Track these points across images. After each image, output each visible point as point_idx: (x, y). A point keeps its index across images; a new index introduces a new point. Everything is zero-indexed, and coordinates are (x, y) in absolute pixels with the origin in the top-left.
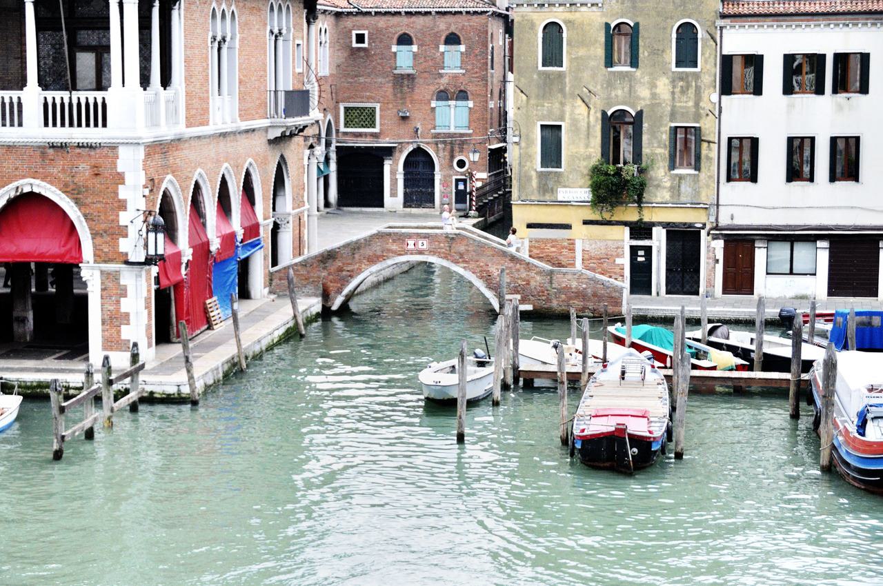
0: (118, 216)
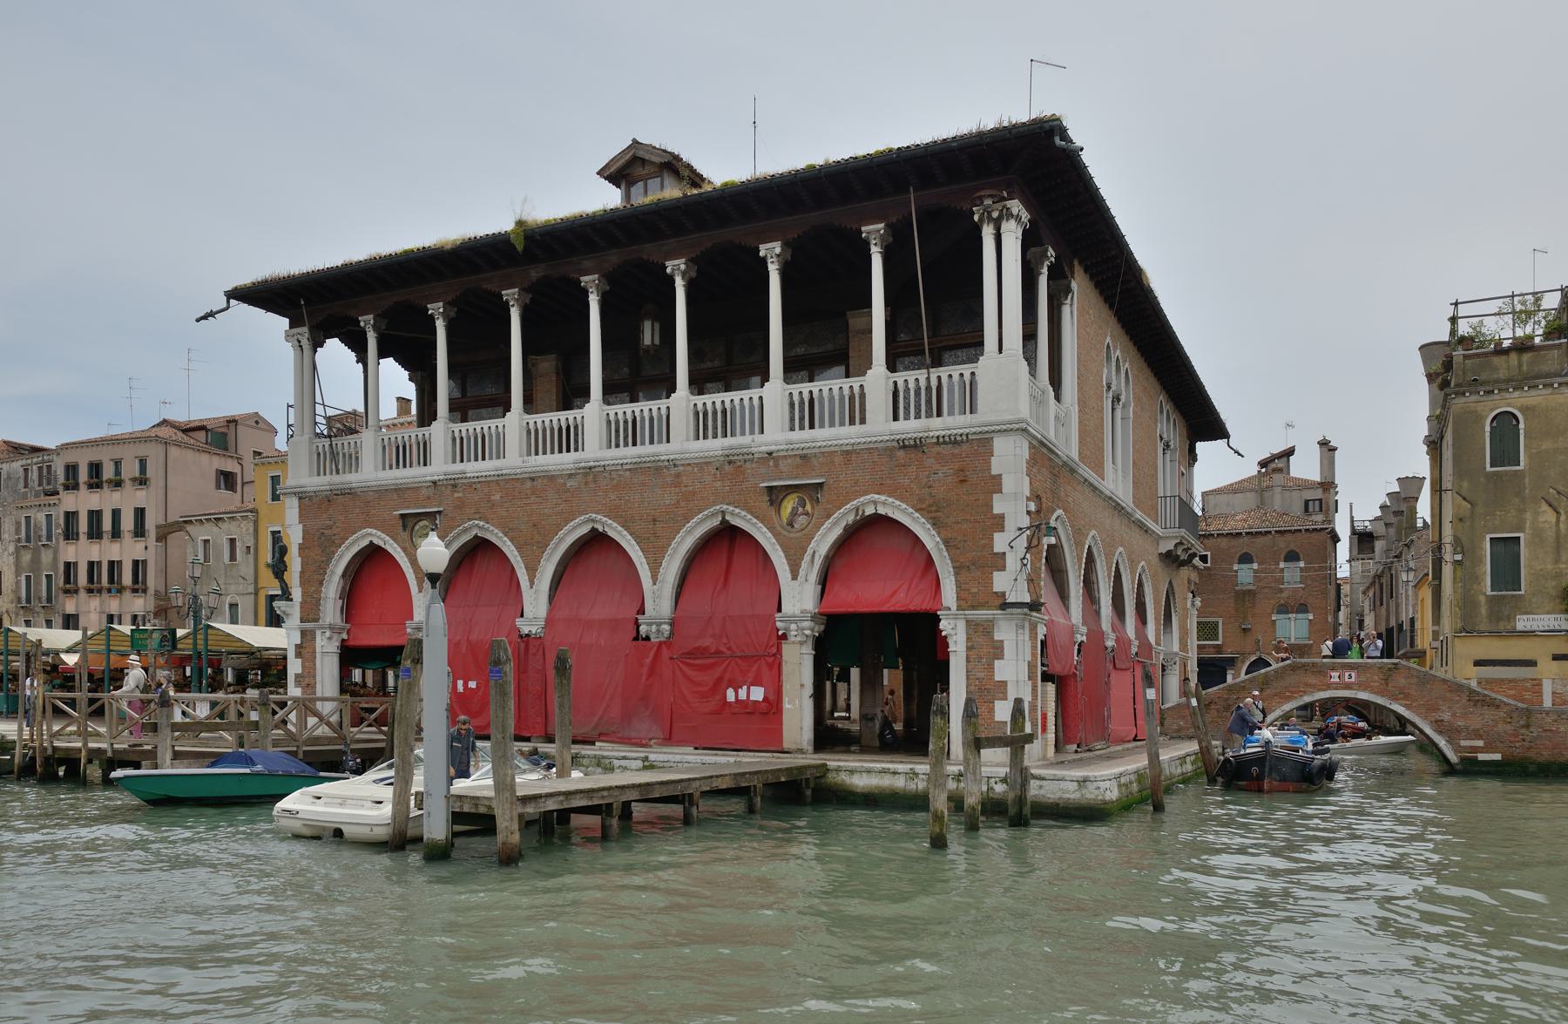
0: (992, 539)
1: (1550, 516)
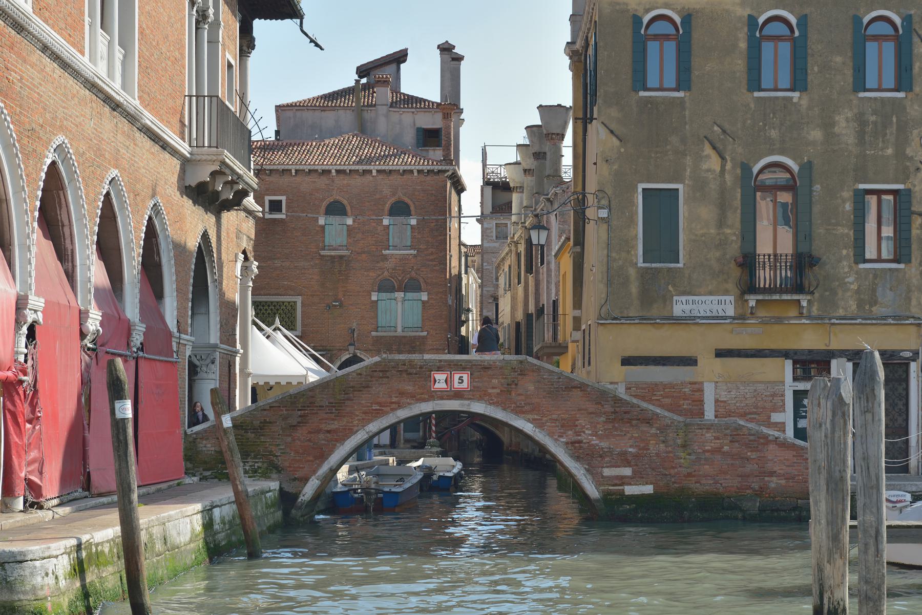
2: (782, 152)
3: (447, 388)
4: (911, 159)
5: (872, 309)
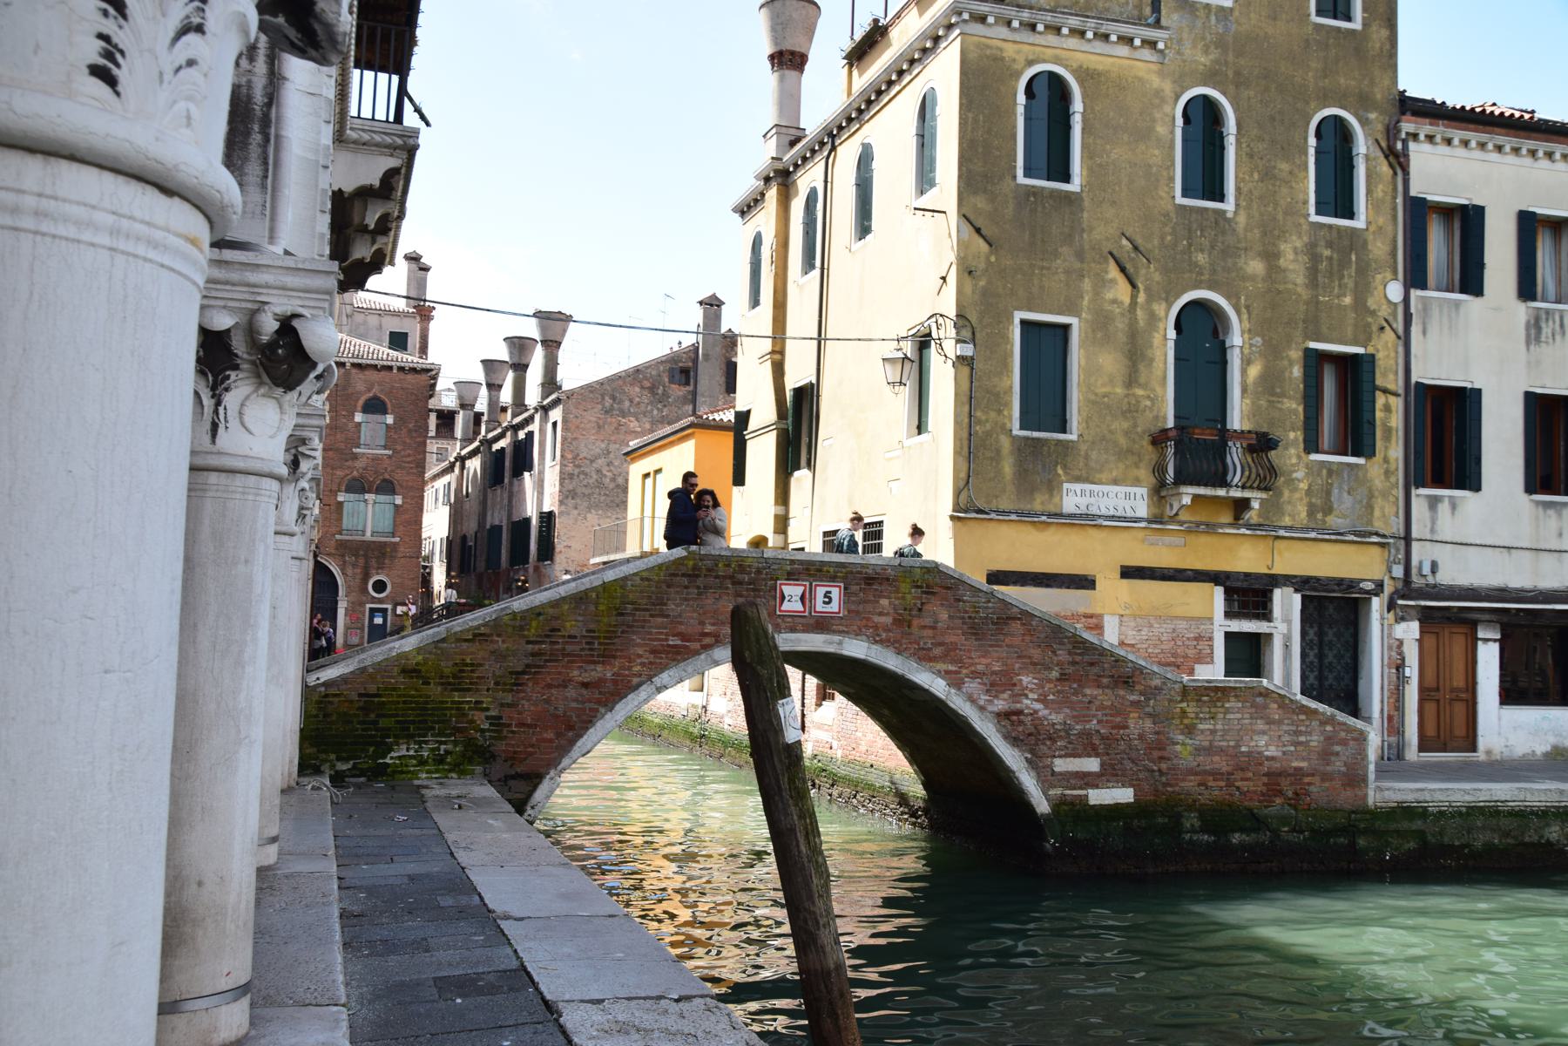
1: (1122, 291)
2: (1212, 286)
3: (804, 612)
4: (1373, 313)
5: (1326, 519)
